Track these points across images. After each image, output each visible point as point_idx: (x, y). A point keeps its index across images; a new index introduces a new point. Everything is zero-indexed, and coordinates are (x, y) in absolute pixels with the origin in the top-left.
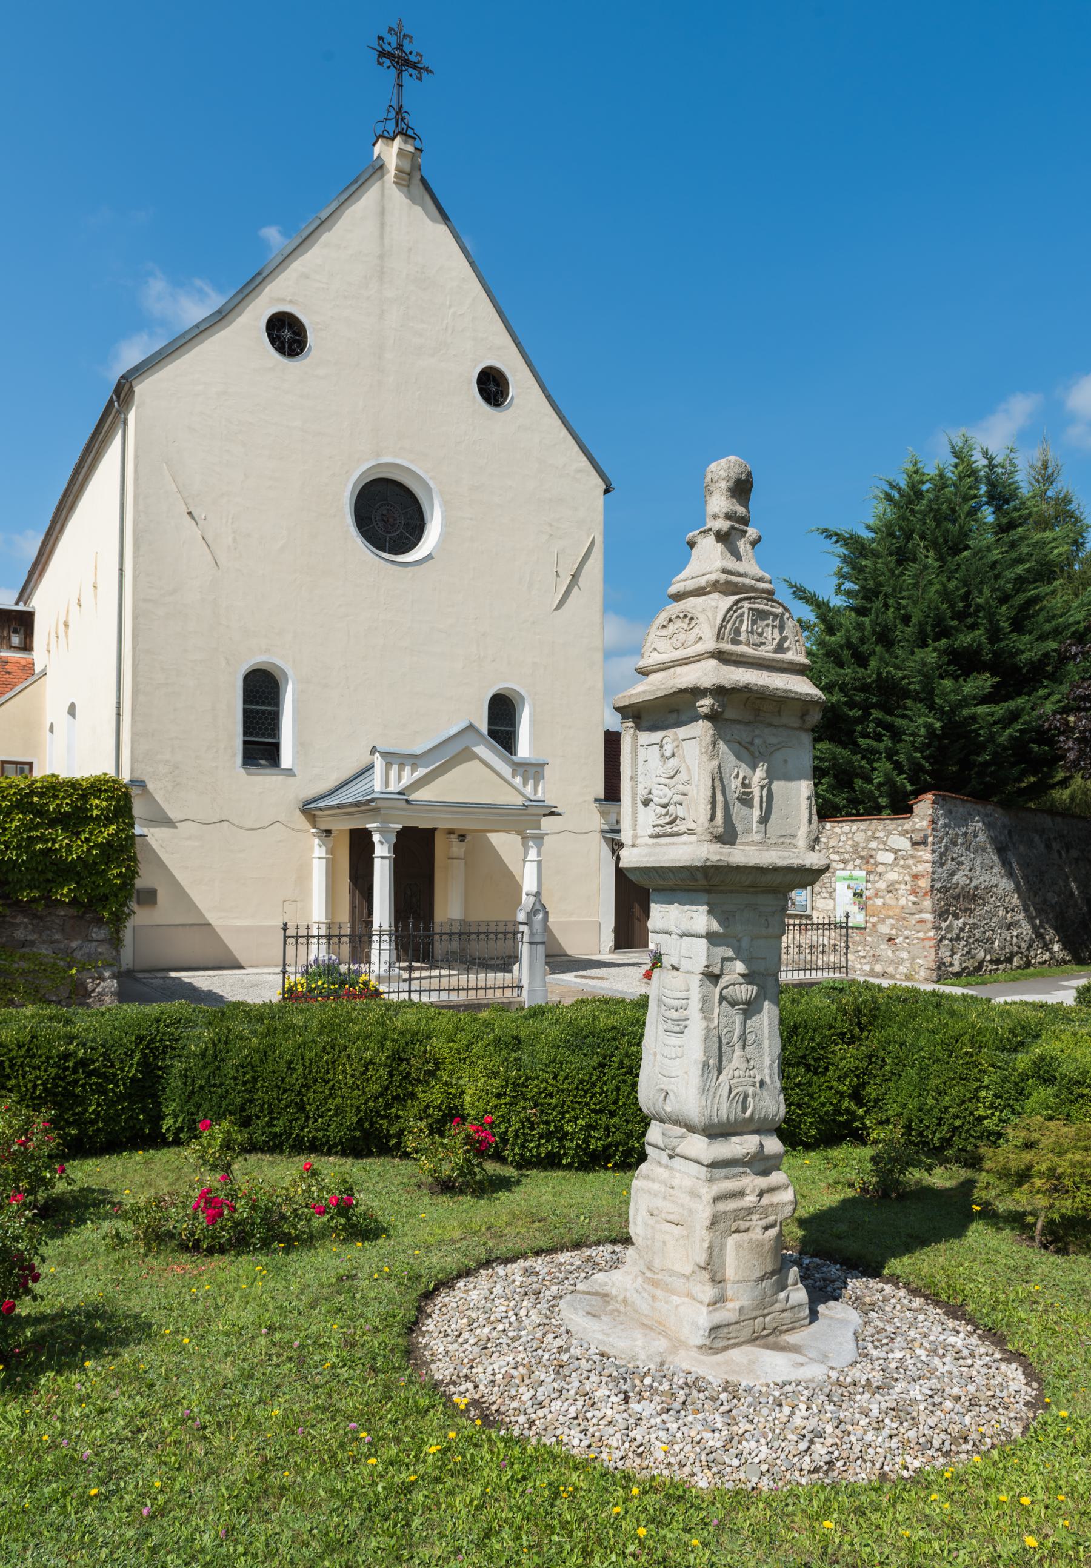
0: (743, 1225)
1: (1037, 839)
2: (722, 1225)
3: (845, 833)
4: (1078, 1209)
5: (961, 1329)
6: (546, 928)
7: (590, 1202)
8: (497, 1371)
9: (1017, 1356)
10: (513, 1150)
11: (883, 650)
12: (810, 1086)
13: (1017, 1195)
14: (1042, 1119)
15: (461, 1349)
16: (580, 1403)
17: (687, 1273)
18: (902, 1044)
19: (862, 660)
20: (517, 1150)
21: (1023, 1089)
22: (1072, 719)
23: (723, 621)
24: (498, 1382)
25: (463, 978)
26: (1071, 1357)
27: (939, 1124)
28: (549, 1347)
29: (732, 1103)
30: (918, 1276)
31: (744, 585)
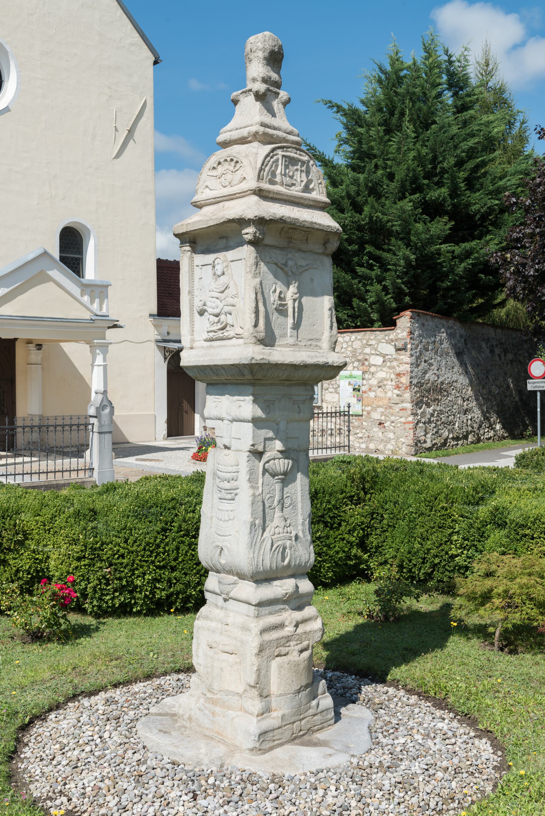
0: (284, 650)
1: (484, 345)
2: (267, 651)
3: (353, 341)
4: (524, 619)
5: (445, 717)
6: (112, 421)
7: (157, 641)
8: (87, 785)
9: (487, 733)
10: (91, 603)
11: (374, 200)
12: (328, 538)
13: (482, 611)
14: (497, 554)
15: (55, 770)
16: (157, 804)
17: (240, 692)
18: (395, 503)
19: (358, 208)
20: (95, 603)
21: (484, 532)
22: (508, 255)
23: (262, 165)
24: (88, 794)
25: (43, 463)
26: (524, 730)
27: (423, 563)
28: (129, 761)
29: (274, 554)
30: (413, 679)
31: (278, 136)
